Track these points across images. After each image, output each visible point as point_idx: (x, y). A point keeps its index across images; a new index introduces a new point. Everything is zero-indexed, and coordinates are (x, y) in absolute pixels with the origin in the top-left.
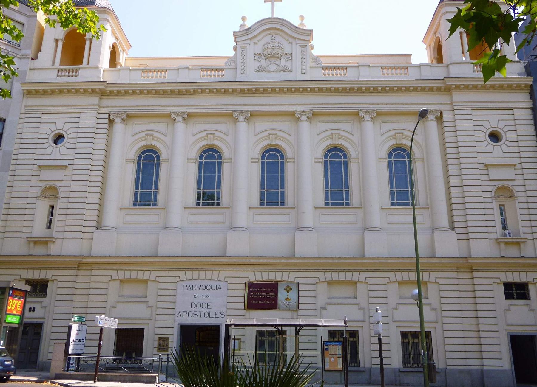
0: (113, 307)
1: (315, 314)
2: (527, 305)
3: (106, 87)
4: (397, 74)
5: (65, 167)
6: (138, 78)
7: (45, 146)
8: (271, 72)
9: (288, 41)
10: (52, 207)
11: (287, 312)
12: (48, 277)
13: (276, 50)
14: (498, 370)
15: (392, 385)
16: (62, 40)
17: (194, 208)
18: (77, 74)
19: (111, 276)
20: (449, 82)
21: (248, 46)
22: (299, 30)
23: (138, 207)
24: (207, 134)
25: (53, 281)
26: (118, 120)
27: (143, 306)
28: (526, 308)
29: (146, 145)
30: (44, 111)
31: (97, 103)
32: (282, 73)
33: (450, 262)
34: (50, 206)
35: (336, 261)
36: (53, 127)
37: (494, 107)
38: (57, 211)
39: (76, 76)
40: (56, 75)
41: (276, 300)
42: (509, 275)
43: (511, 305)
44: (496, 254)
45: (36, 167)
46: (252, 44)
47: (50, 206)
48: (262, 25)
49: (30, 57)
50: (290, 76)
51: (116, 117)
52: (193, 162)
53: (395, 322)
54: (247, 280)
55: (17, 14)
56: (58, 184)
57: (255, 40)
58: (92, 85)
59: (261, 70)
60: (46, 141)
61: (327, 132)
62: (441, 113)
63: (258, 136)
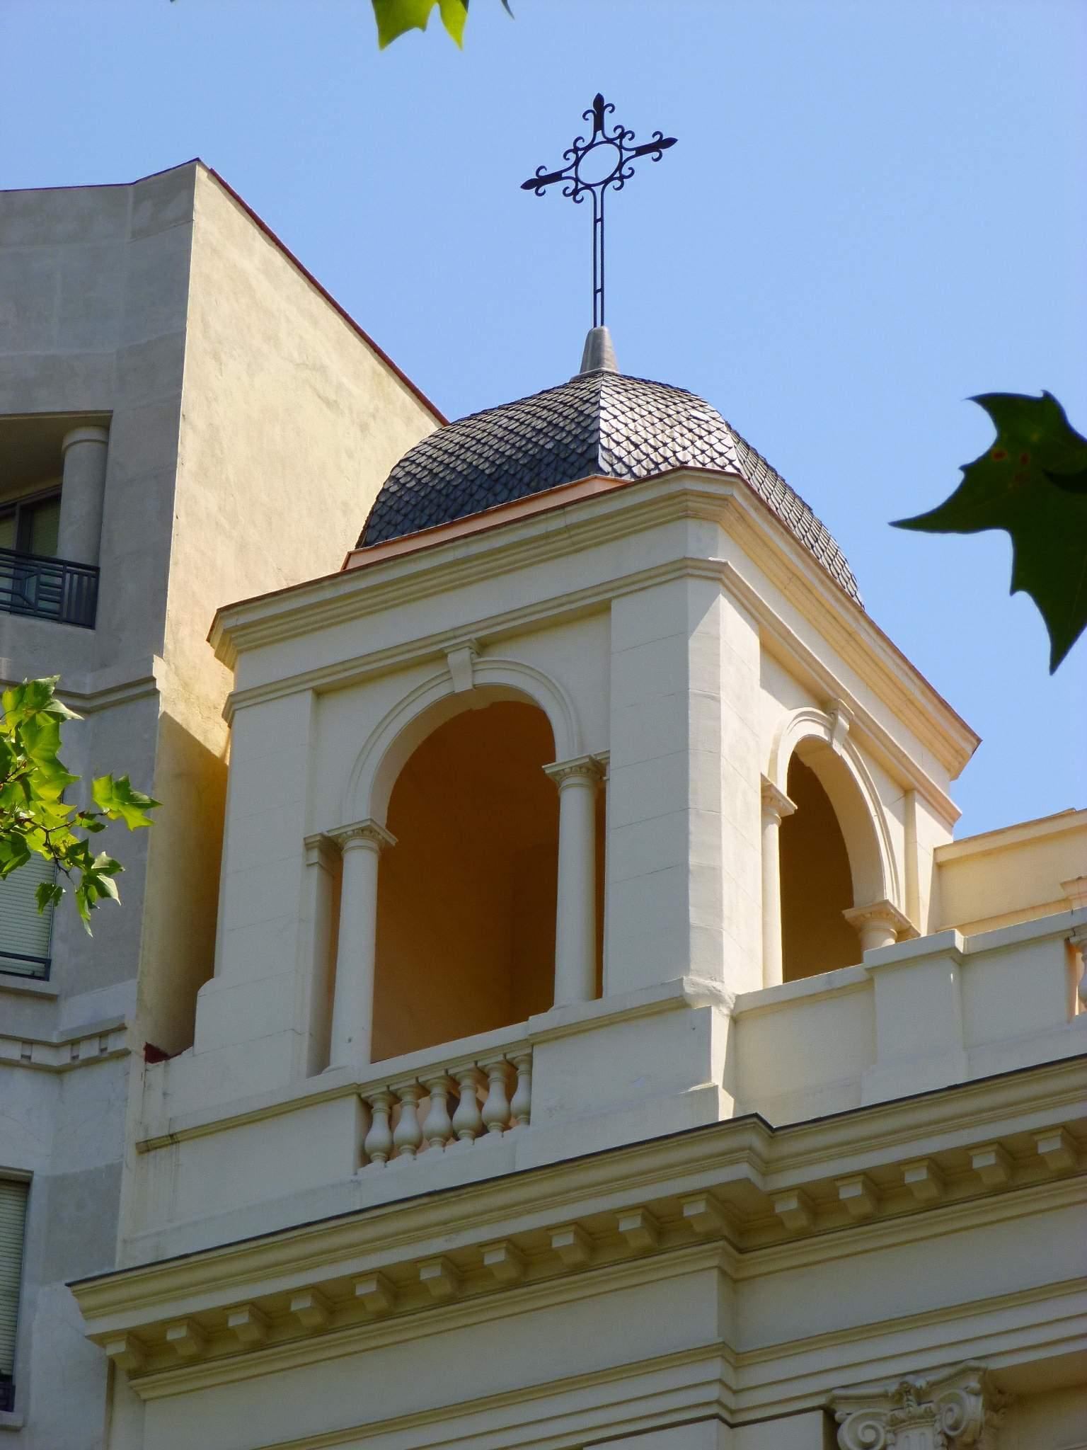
16: (365, 831)
49: (134, 1041)
51: (895, 1425)
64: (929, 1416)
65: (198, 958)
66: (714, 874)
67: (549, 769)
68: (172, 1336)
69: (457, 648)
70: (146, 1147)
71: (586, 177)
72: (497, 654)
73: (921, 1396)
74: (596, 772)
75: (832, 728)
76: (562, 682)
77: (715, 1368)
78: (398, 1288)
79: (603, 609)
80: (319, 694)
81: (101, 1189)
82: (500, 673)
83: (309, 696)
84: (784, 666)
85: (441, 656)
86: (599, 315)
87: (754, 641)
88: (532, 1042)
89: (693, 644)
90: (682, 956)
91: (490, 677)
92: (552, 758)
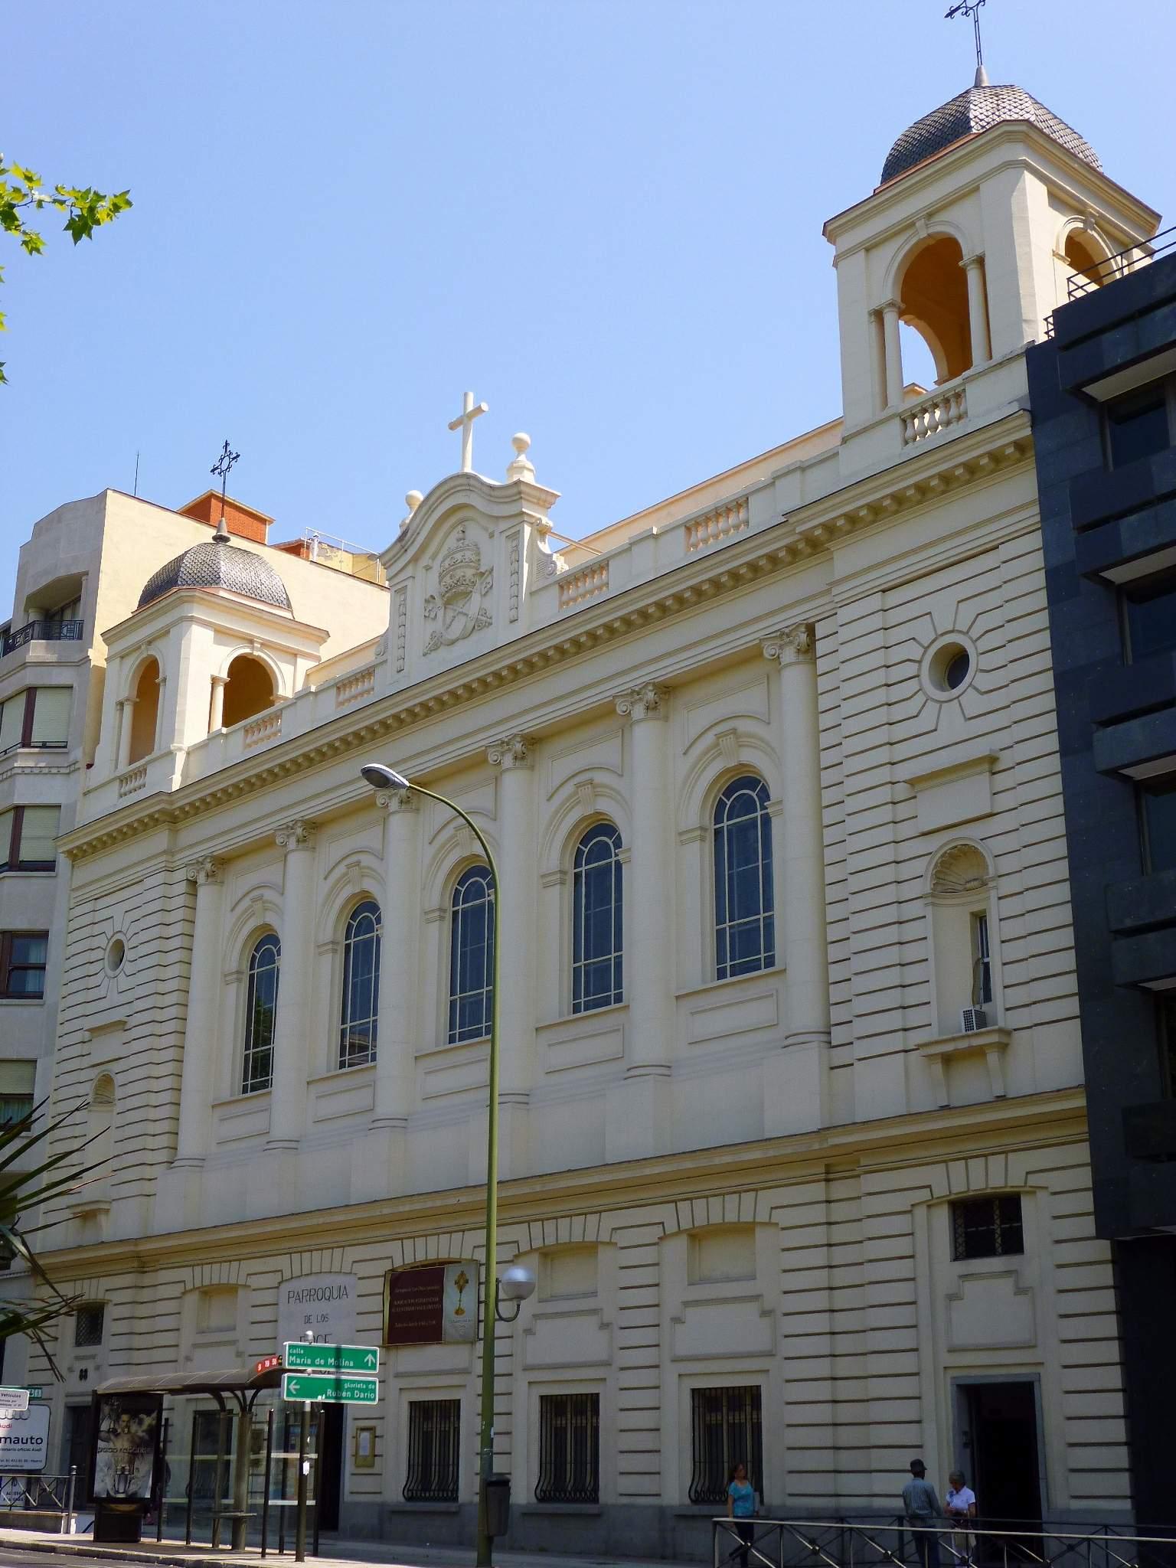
0: (677, 1320)
1: (630, 1339)
2: (1008, 1273)
3: (172, 803)
4: (716, 536)
5: (121, 1025)
6: (328, 709)
7: (911, 707)
8: (453, 642)
9: (486, 529)
10: (980, 920)
11: (461, 1347)
12: (1015, 1181)
13: (459, 573)
14: (651, 1506)
15: (663, 1558)
16: (892, 304)
17: (337, 1076)
18: (962, 408)
19: (929, 1186)
20: (802, 522)
21: (409, 583)
22: (496, 493)
23: (729, 980)
24: (718, 736)
25: (1033, 1191)
26: (201, 879)
27: (227, 1352)
28: (1006, 1286)
29: (728, 770)
30: (97, 893)
31: (164, 846)
32: (475, 636)
33: (789, 1150)
34: (973, 915)
35: (538, 1188)
36: (924, 631)
37: (953, 554)
38: (996, 932)
39: (959, 418)
40: (899, 441)
41: (438, 1313)
42: (393, 1249)
43: (964, 1277)
44: (925, 1102)
45: (902, 791)
46: (420, 572)
47: (973, 915)
48: (441, 500)
49: (82, 765)
50: (501, 634)
51: (781, 647)
52: (692, 840)
53: (676, 1360)
54: (386, 1266)
55: (56, 671)
56: (116, 1067)
57: (425, 560)
58: (914, 472)
59: (437, 643)
60: (913, 685)
61: (336, 870)
62: (811, 630)
63: (555, 797)
64: (791, 642)
65: (97, 741)
66: (183, 712)
67: (961, 264)
68: (932, 484)
69: (919, 219)
70: (85, 794)
71: (970, 5)
72: (937, 218)
73: (788, 636)
74: (980, 261)
75: (253, 648)
76: (967, 228)
77: (164, 858)
78: (876, 511)
79: (977, 189)
80: (867, 250)
81: (73, 808)
82: (941, 226)
83: (863, 253)
84: (1058, 200)
85: (913, 224)
86: (980, 62)
87: (1043, 189)
88: (148, 763)
89: (1013, 201)
90: (172, 740)
91: (931, 231)
92: (961, 258)
